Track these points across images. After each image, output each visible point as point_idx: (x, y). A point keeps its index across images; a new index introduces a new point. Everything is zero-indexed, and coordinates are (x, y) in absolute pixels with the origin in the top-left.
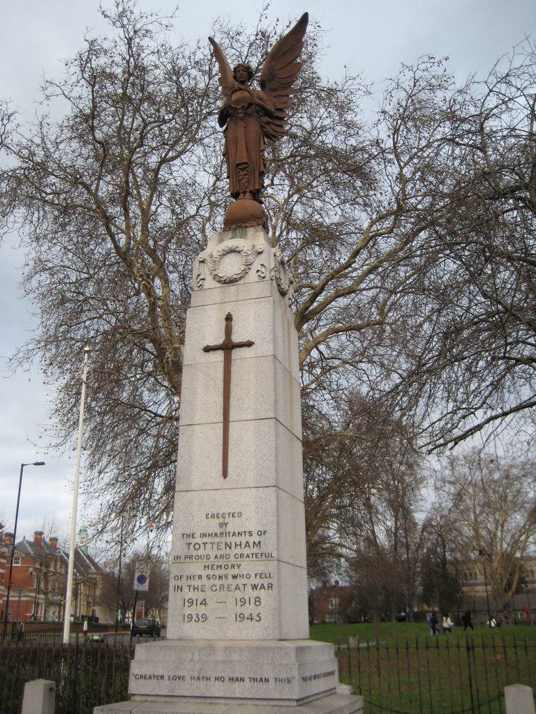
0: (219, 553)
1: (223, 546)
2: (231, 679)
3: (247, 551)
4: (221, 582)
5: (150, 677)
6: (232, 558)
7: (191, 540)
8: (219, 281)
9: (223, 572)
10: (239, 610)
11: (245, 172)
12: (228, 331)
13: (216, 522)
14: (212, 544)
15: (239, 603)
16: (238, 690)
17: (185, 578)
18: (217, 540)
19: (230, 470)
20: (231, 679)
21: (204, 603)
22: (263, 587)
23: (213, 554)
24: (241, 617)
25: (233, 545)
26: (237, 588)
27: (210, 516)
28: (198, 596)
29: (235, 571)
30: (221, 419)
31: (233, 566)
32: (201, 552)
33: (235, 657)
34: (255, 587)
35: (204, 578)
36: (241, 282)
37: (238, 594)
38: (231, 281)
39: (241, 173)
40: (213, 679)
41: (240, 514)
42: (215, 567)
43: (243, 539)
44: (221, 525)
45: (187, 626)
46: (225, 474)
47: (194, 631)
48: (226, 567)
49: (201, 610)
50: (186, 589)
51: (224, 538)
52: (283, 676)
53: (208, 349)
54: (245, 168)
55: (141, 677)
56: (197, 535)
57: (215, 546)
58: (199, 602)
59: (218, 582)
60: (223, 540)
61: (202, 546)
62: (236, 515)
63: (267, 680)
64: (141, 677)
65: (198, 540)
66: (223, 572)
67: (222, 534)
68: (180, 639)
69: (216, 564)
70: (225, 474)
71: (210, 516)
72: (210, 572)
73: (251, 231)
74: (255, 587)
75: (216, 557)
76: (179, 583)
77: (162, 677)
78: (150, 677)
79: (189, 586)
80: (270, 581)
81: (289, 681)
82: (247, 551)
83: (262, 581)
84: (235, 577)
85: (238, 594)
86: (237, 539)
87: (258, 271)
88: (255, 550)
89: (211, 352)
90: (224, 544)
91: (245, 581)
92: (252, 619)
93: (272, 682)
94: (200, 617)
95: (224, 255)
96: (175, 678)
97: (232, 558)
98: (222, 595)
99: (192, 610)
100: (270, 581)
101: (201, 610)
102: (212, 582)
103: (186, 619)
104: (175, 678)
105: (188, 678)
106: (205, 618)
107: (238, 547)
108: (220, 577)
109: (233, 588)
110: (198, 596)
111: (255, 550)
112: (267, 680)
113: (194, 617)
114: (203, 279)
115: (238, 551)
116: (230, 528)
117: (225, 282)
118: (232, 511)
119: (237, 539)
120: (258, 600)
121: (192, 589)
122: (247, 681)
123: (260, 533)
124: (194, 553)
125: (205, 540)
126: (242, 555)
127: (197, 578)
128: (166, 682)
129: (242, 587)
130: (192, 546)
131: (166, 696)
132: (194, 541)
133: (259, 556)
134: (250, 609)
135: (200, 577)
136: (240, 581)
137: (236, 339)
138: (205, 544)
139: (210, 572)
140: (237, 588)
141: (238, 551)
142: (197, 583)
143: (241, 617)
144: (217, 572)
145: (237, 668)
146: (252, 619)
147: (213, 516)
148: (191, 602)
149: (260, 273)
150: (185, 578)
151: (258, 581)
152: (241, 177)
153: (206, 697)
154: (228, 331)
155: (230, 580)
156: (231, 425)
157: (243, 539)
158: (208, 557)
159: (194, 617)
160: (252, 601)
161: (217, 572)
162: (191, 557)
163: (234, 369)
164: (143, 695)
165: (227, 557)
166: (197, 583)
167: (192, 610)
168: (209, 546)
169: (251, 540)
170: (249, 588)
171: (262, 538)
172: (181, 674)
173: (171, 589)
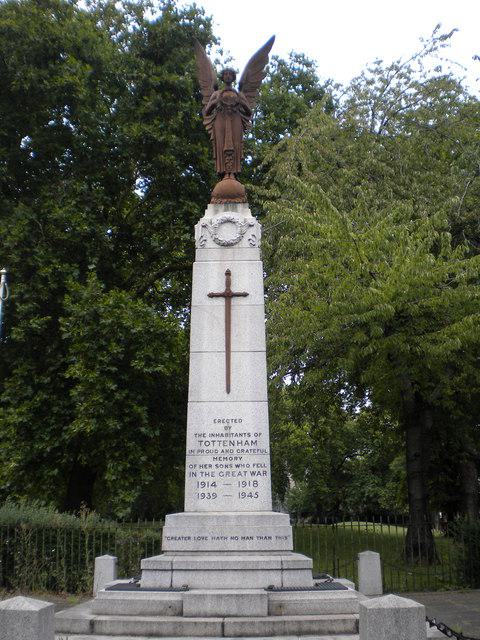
0: (225, 449)
3: (246, 448)
4: (227, 470)
7: (202, 438)
8: (219, 244)
9: (228, 462)
10: (241, 490)
12: (228, 283)
13: (222, 425)
16: (248, 545)
18: (223, 439)
19: (232, 388)
21: (214, 485)
24: (243, 495)
26: (240, 474)
28: (207, 479)
29: (238, 462)
31: (236, 458)
32: (210, 448)
34: (253, 473)
44: (226, 428)
46: (228, 390)
47: (204, 504)
49: (212, 490)
53: (212, 296)
59: (224, 470)
66: (228, 462)
70: (228, 390)
72: (218, 462)
73: (240, 207)
74: (253, 473)
77: (189, 538)
82: (246, 448)
84: (237, 466)
86: (239, 439)
88: (253, 447)
91: (245, 469)
93: (274, 538)
96: (199, 538)
99: (206, 490)
101: (212, 490)
102: (220, 469)
104: (199, 538)
105: (210, 538)
110: (210, 480)
111: (253, 447)
115: (240, 447)
116: (232, 431)
117: (223, 245)
119: (239, 439)
120: (256, 483)
123: (256, 435)
124: (205, 448)
125: (213, 439)
132: (204, 439)
134: (250, 489)
135: (210, 466)
139: (218, 462)
140: (240, 474)
141: (240, 447)
142: (209, 470)
143: (243, 495)
144: (224, 463)
151: (255, 469)
154: (228, 283)
157: (244, 439)
158: (216, 451)
161: (224, 463)
165: (232, 451)
167: (206, 490)
168: (216, 444)
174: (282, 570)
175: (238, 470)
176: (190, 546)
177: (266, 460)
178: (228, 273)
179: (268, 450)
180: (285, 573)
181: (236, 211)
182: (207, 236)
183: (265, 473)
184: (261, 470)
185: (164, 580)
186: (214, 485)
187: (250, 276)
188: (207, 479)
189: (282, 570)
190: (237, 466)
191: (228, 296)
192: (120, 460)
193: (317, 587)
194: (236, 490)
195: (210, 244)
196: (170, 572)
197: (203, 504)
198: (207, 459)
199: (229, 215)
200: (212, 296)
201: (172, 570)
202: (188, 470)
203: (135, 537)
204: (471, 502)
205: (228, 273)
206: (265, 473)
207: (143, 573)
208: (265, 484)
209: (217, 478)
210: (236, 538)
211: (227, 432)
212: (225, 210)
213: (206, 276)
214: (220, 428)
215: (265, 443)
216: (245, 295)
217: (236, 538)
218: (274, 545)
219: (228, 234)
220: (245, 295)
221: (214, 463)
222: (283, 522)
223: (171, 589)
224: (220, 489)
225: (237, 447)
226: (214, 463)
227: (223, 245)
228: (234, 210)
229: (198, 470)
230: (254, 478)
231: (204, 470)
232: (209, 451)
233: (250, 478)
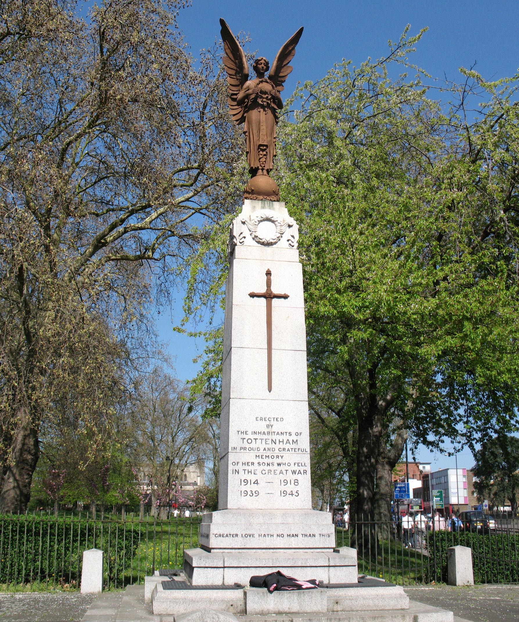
0: (267, 447)
1: (269, 441)
2: (289, 536)
3: (287, 446)
4: (269, 468)
5: (227, 536)
6: (277, 451)
7: (244, 436)
8: (258, 242)
9: (270, 461)
10: (283, 488)
11: (265, 153)
12: (269, 284)
13: (264, 424)
14: (262, 439)
15: (283, 483)
16: (294, 542)
17: (240, 464)
18: (265, 437)
20: (289, 536)
21: (256, 482)
22: (299, 472)
23: (262, 447)
24: (285, 493)
25: (277, 442)
26: (281, 472)
27: (259, 419)
28: (249, 477)
29: (280, 460)
30: (266, 347)
32: (253, 445)
33: (290, 520)
34: (294, 472)
35: (256, 464)
36: (274, 246)
37: (282, 477)
38: (269, 244)
39: (261, 152)
40: (275, 536)
41: (282, 419)
42: (264, 457)
43: (285, 438)
44: (268, 426)
45: (243, 499)
46: (270, 390)
47: (247, 502)
48: (273, 457)
49: (254, 487)
50: (241, 472)
51: (270, 436)
52: (325, 532)
53: (252, 295)
54: (265, 149)
55: (220, 535)
56: (249, 433)
57: (264, 442)
58: (252, 482)
59: (267, 468)
60: (270, 437)
61: (254, 441)
62: (279, 420)
63: (314, 535)
64: (220, 535)
65: (250, 436)
66: (270, 461)
67: (269, 433)
68: (239, 509)
69: (265, 455)
70: (270, 390)
71: (259, 419)
72: (261, 461)
73: (276, 204)
74: (294, 472)
75: (265, 449)
76: (236, 468)
77: (237, 535)
78: (227, 536)
79: (245, 470)
80: (305, 468)
81: (329, 536)
82: (287, 446)
83: (299, 468)
84: (279, 464)
85: (282, 477)
86: (281, 437)
87: (288, 240)
88: (294, 446)
89: (255, 298)
90: (270, 441)
91: (287, 468)
92: (292, 494)
93: (317, 536)
94: (254, 492)
95: (261, 221)
96: (246, 536)
97: (277, 451)
98: (271, 476)
99: (248, 488)
100: (305, 468)
101: (254, 487)
102: (262, 467)
103: (243, 494)
104: (246, 536)
105: (256, 536)
106: (257, 493)
107: (281, 443)
108: (268, 464)
109: (278, 472)
110: (253, 478)
111: (294, 446)
112: (314, 535)
113: (249, 493)
114: (245, 237)
115: (281, 446)
116: (274, 429)
117: (263, 244)
118: (276, 417)
119: (281, 437)
120: (296, 482)
121: (246, 472)
122: (300, 536)
123: (297, 434)
124: (248, 446)
125: (256, 436)
126: (284, 449)
127: (250, 464)
128: (240, 538)
129: (284, 472)
130: (245, 441)
131: (239, 549)
132: (247, 437)
133: (297, 450)
134: (290, 488)
135: (253, 464)
136: (283, 468)
137: (275, 290)
138: (256, 439)
139: (261, 461)
140: (281, 472)
141: (281, 446)
142: (251, 468)
143: (285, 493)
144: (266, 461)
145: (293, 528)
146: (292, 494)
147: (261, 419)
148: (246, 482)
149: (290, 242)
150: (240, 464)
151: (296, 468)
152: (261, 156)
153: (270, 549)
154: (269, 284)
155: (276, 467)
156: (273, 352)
157: (285, 438)
158: (258, 449)
159: (249, 493)
160: (293, 482)
161: (266, 461)
162: (245, 449)
163: (273, 313)
164: (221, 548)
165: (273, 450)
166: (251, 468)
167: (248, 488)
168: (259, 441)
169: (291, 439)
170: (290, 473)
171: (298, 438)
172: (250, 533)
173: (230, 472)
174: (329, 566)
175: (279, 468)
176: (238, 542)
177: (306, 459)
178: (268, 273)
179: (308, 450)
180: (331, 568)
181: (274, 209)
182: (246, 233)
183: (305, 472)
184: (302, 469)
185: (214, 577)
186: (256, 482)
187: (290, 278)
188: (249, 477)
189: (329, 566)
190: (279, 464)
191: (269, 296)
192: (102, 487)
193: (362, 583)
194: (279, 487)
195: (249, 241)
196: (222, 569)
197: (247, 502)
198: (249, 457)
199: (267, 212)
200: (252, 295)
201: (224, 567)
202: (231, 468)
203: (188, 282)
204: (502, 509)
205: (268, 273)
206: (305, 472)
207: (195, 569)
208: (305, 481)
209: (259, 476)
210: (282, 536)
211: (269, 430)
212: (263, 208)
213: (247, 272)
214: (262, 426)
215: (305, 442)
216: (285, 297)
217: (282, 536)
218: (317, 542)
219: (267, 232)
220: (285, 297)
221: (256, 461)
222: (325, 521)
223: (224, 587)
224: (261, 488)
225: (278, 446)
226: (256, 461)
227: (273, 222)
228: (271, 207)
229: (240, 467)
230: (295, 476)
231: (246, 467)
232: (251, 449)
233: (291, 477)
